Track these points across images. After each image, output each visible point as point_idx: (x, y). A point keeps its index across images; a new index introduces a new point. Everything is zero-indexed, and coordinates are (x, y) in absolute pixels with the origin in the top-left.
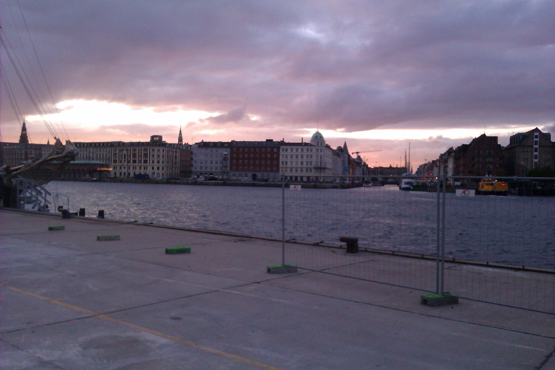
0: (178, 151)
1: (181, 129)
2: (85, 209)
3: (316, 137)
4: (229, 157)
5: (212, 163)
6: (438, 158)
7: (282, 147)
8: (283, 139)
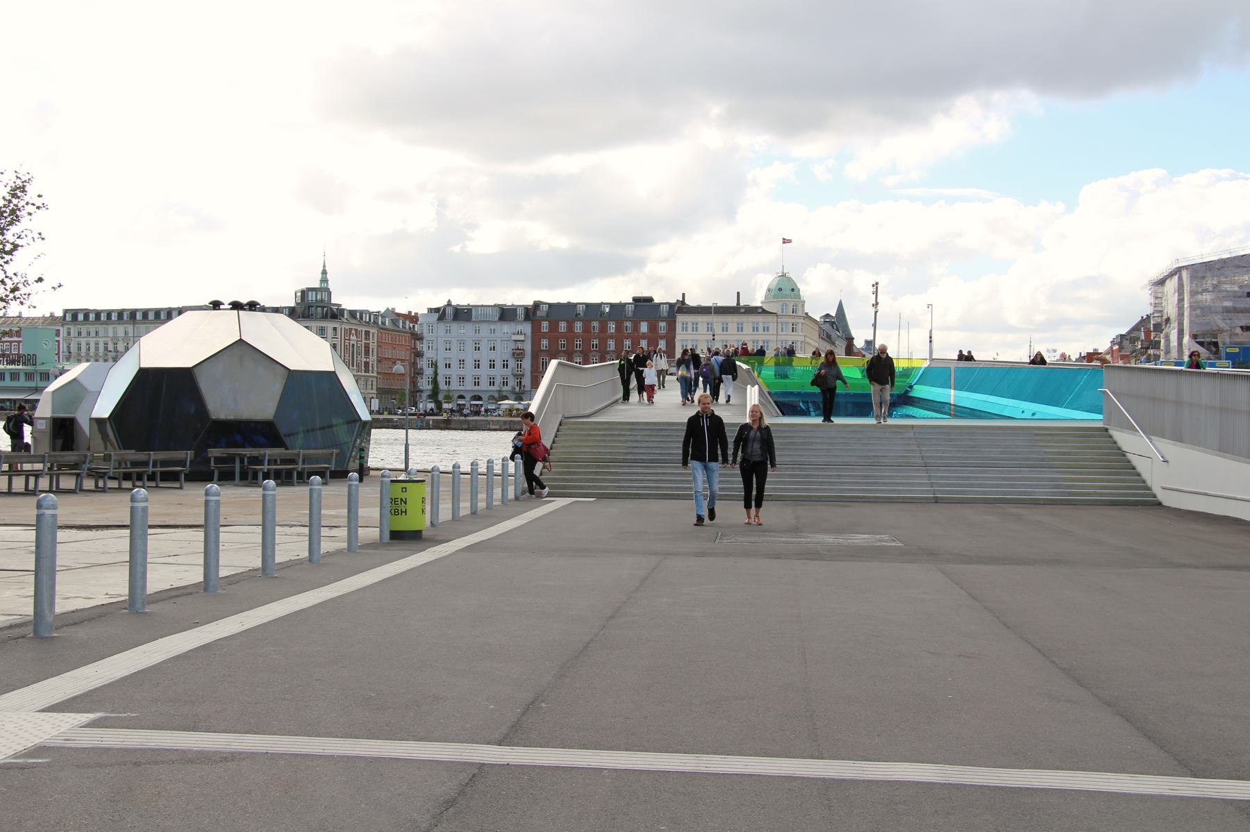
0: (373, 331)
1: (324, 266)
2: (58, 516)
3: (780, 290)
4: (528, 347)
5: (492, 366)
6: (383, 311)
7: (681, 319)
8: (684, 295)
